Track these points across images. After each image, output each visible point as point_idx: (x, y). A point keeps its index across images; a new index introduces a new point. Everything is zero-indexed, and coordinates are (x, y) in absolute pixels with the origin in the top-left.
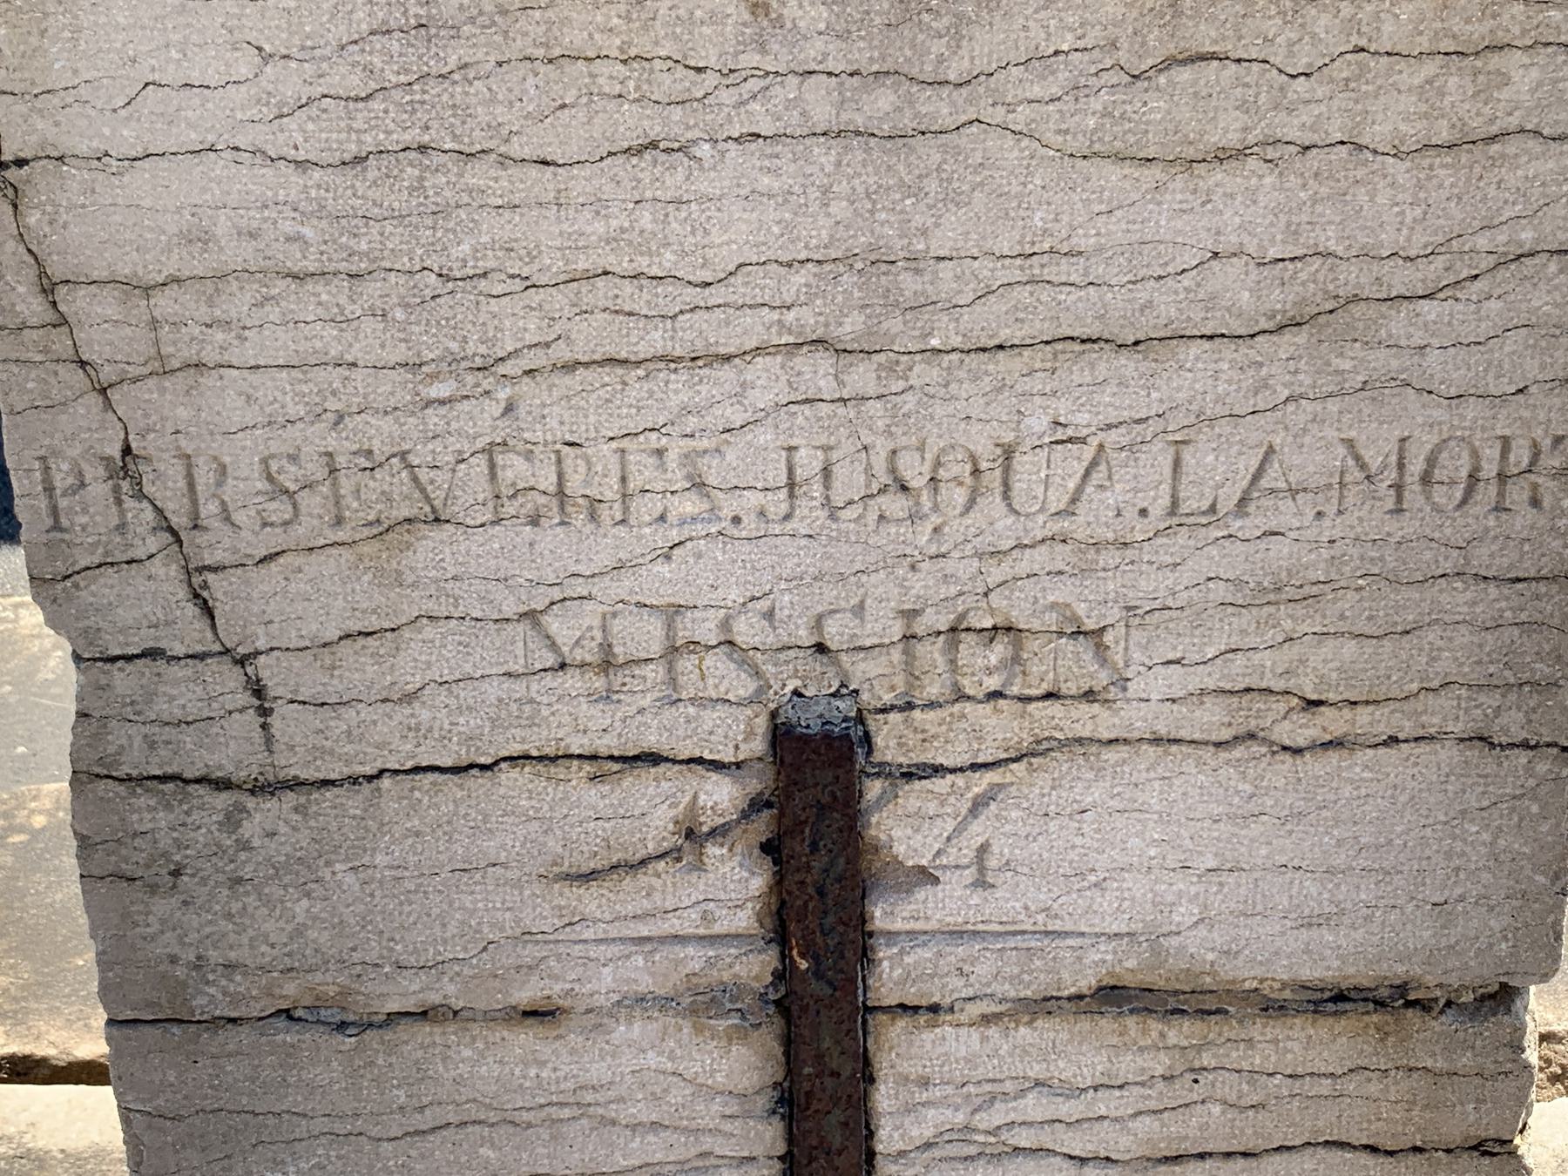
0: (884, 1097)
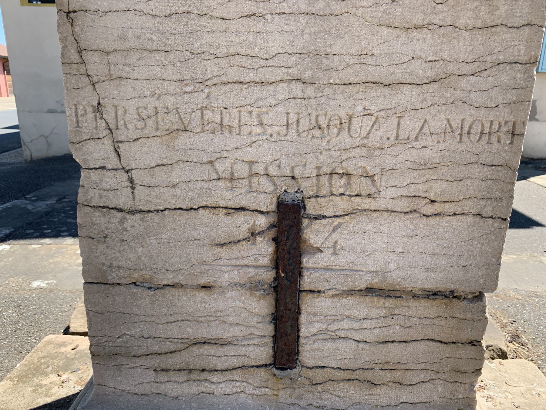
0: (303, 319)
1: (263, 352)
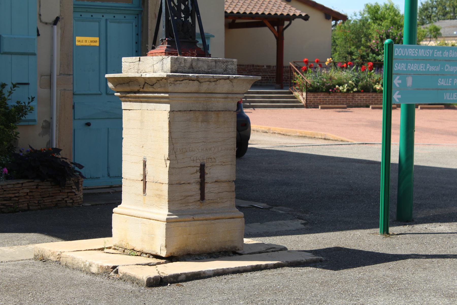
0: (205, 189)
1: (198, 197)
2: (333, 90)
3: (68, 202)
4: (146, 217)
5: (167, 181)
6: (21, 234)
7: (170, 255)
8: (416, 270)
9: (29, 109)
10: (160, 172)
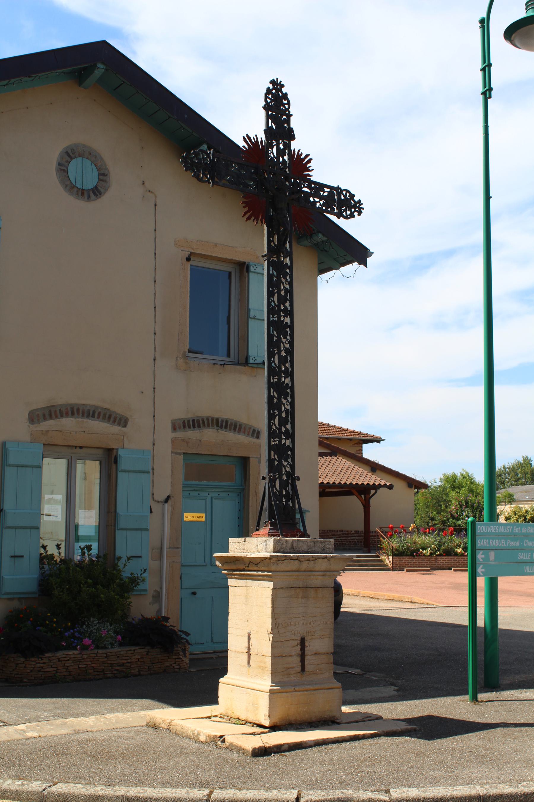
1: (299, 669)
2: (417, 553)
3: (175, 667)
4: (250, 687)
5: (269, 653)
6: (133, 700)
7: (272, 724)
8: (506, 740)
9: (141, 580)
10: (264, 646)
